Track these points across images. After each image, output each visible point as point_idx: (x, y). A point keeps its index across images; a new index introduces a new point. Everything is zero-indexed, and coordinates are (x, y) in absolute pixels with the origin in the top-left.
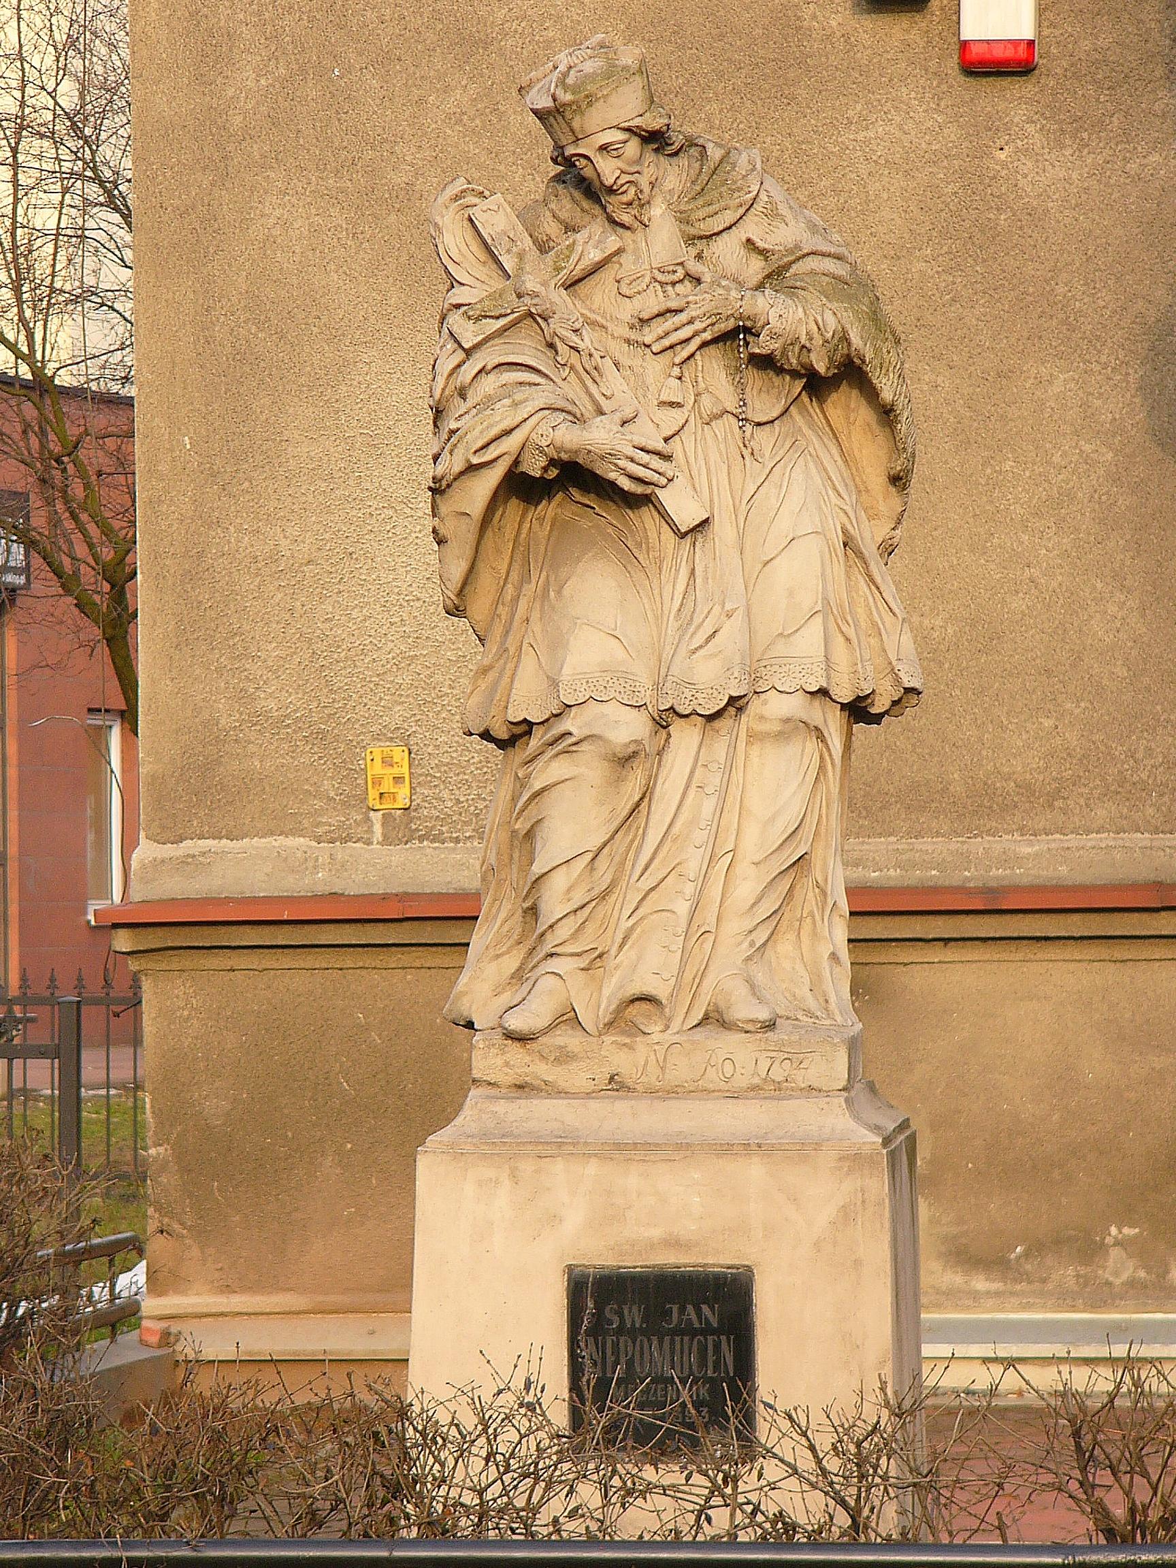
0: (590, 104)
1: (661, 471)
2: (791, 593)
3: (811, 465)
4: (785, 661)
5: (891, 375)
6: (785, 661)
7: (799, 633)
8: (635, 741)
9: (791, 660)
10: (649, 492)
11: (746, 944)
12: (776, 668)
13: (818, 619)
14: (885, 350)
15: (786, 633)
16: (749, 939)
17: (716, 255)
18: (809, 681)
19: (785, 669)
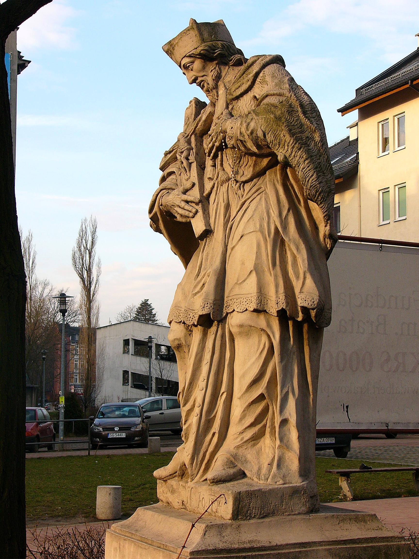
0: (173, 49)
1: (189, 210)
2: (243, 263)
3: (263, 199)
4: (239, 296)
5: (286, 147)
6: (239, 296)
7: (246, 282)
8: (177, 339)
9: (242, 296)
10: (188, 221)
11: (239, 439)
12: (235, 300)
13: (254, 274)
14: (282, 135)
15: (238, 283)
16: (241, 437)
17: (239, 106)
18: (250, 306)
19: (239, 300)
